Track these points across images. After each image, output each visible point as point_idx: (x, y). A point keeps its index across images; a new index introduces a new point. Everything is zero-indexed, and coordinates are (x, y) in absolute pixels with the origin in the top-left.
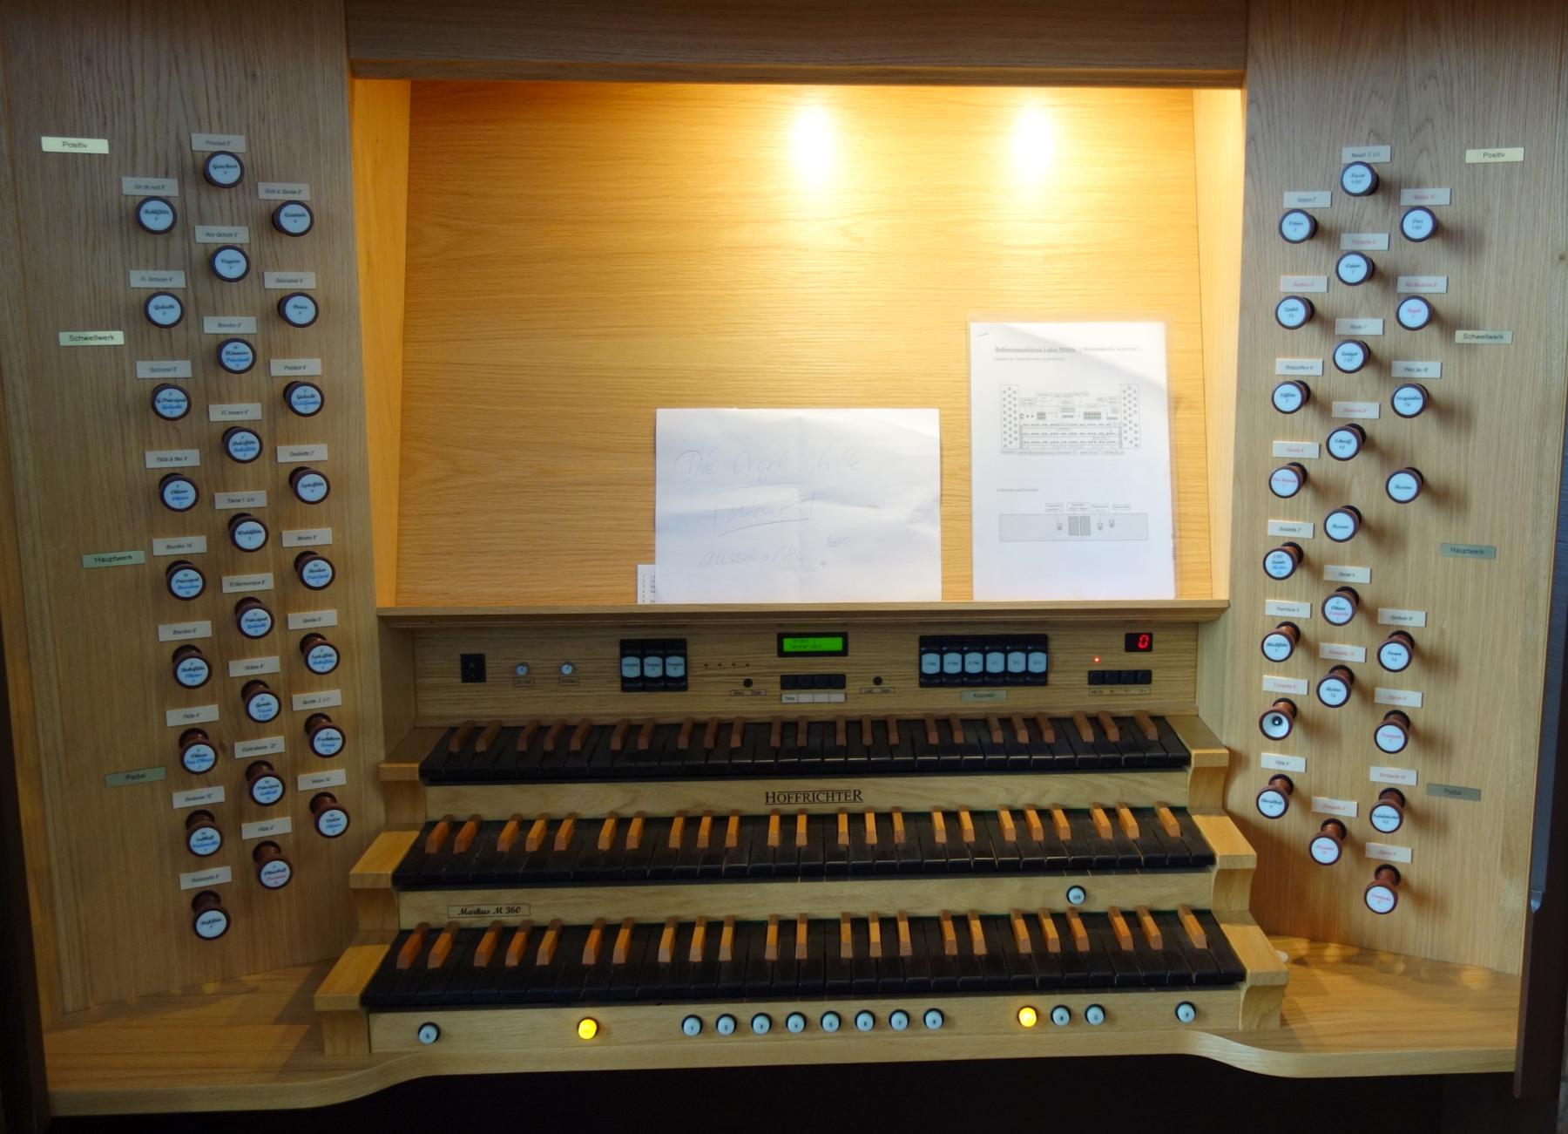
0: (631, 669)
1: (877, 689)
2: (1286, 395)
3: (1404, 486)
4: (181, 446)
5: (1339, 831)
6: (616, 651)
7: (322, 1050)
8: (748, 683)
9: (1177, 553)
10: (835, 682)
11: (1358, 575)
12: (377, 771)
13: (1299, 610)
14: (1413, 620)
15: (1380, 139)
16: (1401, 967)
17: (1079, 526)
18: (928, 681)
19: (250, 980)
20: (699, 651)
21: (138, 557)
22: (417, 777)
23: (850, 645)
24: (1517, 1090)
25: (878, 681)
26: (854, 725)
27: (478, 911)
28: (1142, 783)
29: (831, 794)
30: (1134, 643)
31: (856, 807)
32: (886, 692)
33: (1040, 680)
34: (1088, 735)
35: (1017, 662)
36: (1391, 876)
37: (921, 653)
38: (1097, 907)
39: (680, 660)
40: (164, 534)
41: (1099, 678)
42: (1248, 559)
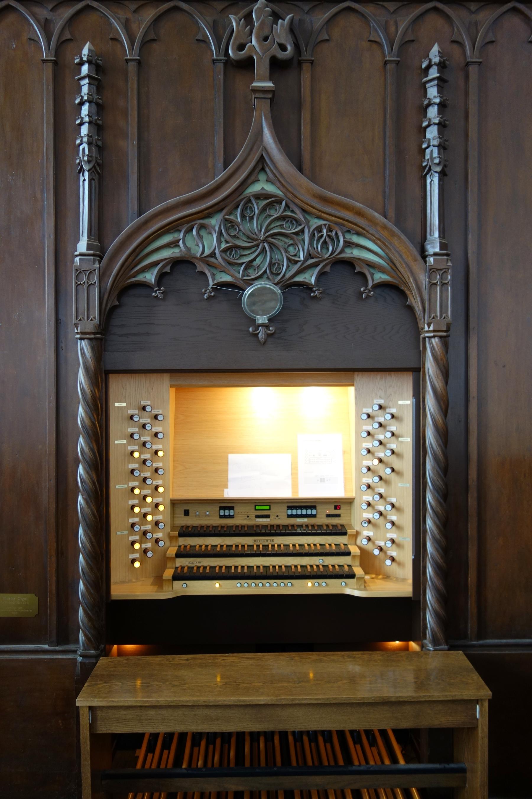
0: (222, 513)
1: (277, 518)
2: (364, 452)
3: (389, 471)
4: (135, 463)
5: (381, 549)
6: (218, 509)
7: (163, 589)
8: (248, 517)
9: (345, 487)
10: (268, 516)
11: (382, 491)
12: (169, 533)
13: (370, 499)
14: (394, 500)
15: (381, 398)
16: (395, 579)
17: (322, 480)
18: (289, 516)
19: (142, 579)
20: (238, 508)
21: (126, 486)
22: (177, 535)
23: (271, 508)
24: (412, 599)
25: (277, 516)
26: (272, 526)
27: (192, 563)
28: (337, 538)
29: (267, 540)
30: (336, 508)
31: (273, 543)
32: (279, 519)
33: (314, 516)
34: (325, 528)
35: (309, 512)
36: (393, 559)
37: (287, 510)
38: (326, 564)
39: (233, 511)
40: (131, 482)
41: (328, 516)
42: (359, 488)
